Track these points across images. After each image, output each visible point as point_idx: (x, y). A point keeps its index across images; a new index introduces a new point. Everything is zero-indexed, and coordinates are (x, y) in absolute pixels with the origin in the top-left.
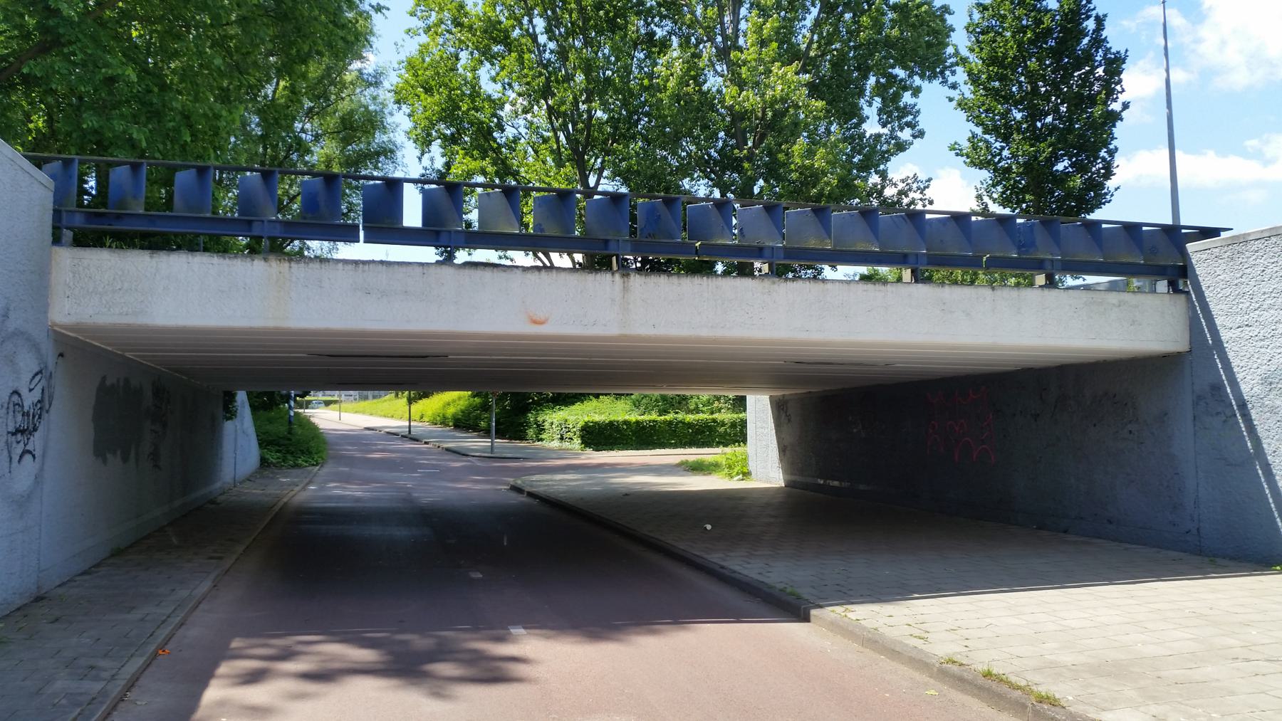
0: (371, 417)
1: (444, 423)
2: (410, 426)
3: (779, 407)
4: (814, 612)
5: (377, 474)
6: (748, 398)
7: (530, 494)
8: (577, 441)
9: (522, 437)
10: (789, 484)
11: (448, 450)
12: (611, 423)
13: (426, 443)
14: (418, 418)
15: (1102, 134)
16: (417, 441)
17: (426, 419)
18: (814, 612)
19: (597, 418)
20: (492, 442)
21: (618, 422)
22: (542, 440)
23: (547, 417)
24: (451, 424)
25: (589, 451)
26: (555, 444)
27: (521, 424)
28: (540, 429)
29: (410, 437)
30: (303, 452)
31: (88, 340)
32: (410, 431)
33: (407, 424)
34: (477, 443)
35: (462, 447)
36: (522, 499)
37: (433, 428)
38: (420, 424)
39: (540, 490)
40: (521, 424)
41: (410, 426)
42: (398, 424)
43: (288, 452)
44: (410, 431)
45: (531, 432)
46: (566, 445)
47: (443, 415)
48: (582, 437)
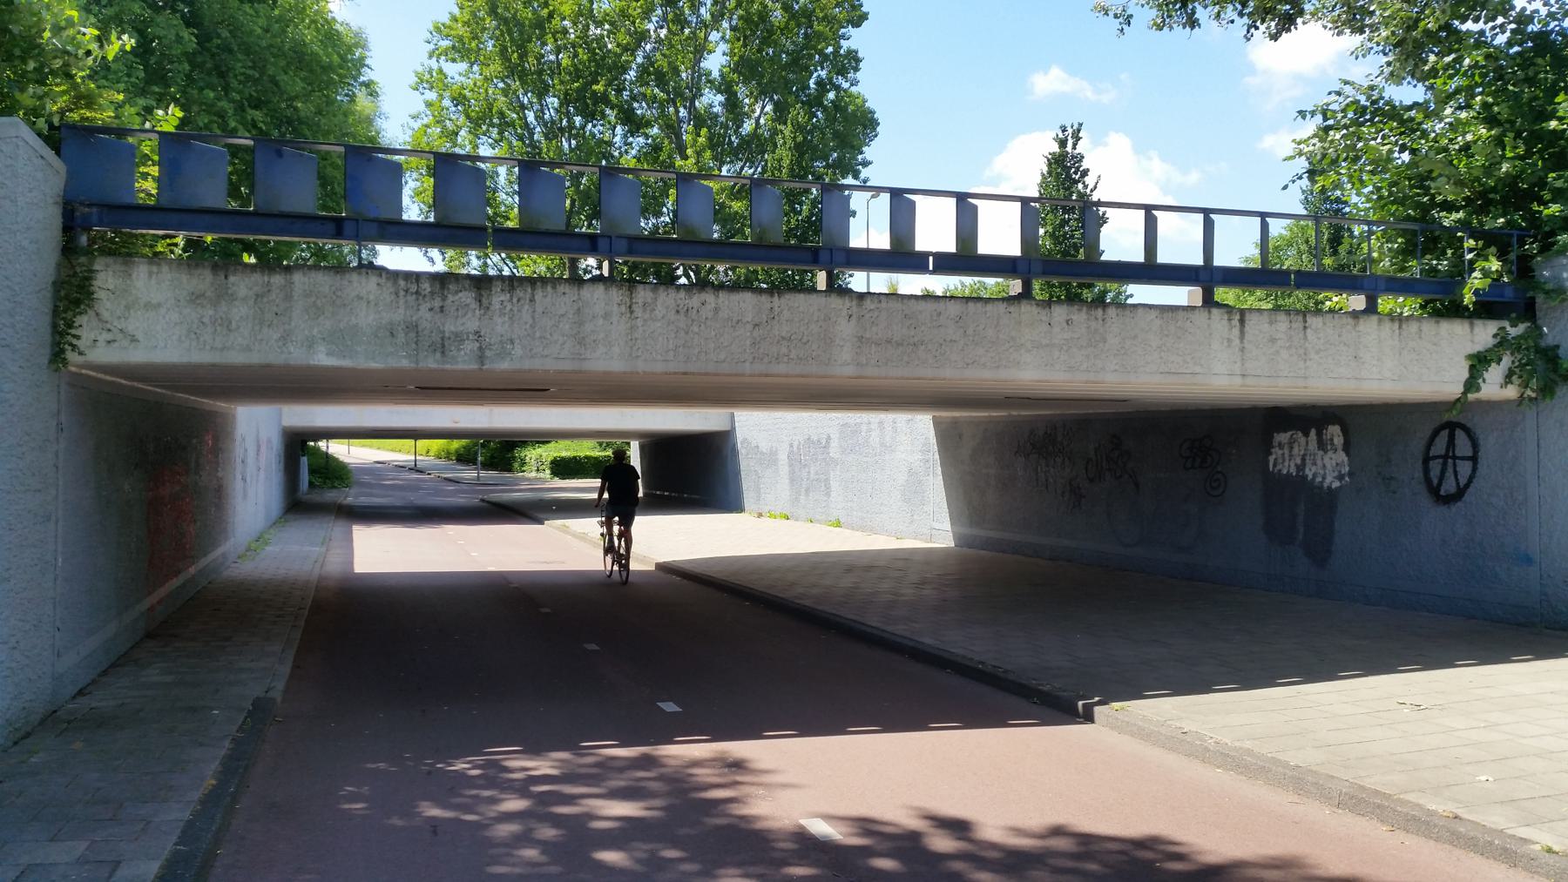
0: (378, 451)
1: (448, 458)
2: (416, 460)
3: (642, 448)
4: (546, 522)
5: (390, 493)
6: (632, 443)
7: (488, 502)
8: (548, 472)
9: (510, 470)
10: (961, 541)
11: (446, 479)
12: (575, 458)
13: (429, 474)
14: (424, 453)
15: (1422, 54)
16: (422, 472)
17: (431, 453)
18: (546, 522)
19: (564, 454)
20: (478, 473)
21: (580, 457)
22: (524, 471)
23: (528, 453)
24: (454, 458)
25: (556, 479)
26: (534, 474)
27: (509, 459)
28: (523, 463)
29: (415, 469)
30: (337, 478)
31: (84, 371)
32: (416, 465)
33: (413, 458)
34: (469, 474)
35: (457, 477)
36: (484, 504)
37: (438, 462)
38: (427, 458)
39: (494, 500)
40: (509, 459)
41: (416, 460)
42: (440, 267)
43: (327, 478)
44: (416, 465)
45: (516, 465)
46: (541, 475)
47: (447, 450)
48: (552, 469)
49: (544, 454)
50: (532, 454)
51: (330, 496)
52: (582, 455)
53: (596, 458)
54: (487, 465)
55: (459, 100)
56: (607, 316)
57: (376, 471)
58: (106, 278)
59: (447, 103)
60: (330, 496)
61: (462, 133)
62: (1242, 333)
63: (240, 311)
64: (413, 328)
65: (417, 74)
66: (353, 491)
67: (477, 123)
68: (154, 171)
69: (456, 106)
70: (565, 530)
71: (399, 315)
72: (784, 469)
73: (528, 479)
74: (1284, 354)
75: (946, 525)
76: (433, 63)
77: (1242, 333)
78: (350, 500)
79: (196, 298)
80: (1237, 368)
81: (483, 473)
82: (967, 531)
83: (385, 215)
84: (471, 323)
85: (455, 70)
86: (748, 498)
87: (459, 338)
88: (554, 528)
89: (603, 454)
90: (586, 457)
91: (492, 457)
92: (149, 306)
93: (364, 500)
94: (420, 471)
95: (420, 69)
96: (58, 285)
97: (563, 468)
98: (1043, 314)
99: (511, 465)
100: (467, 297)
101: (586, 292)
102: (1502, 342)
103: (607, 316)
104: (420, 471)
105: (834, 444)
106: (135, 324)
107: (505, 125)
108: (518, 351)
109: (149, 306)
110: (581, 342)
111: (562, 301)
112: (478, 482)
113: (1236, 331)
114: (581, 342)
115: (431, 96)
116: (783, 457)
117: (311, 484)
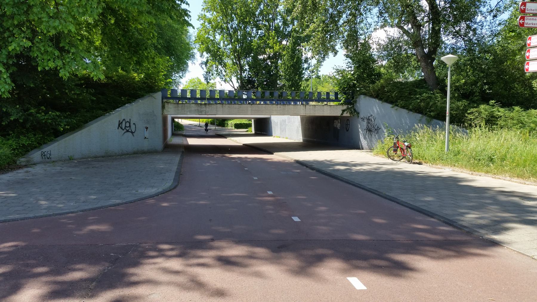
8: (234, 127)
10: (303, 140)
19: (238, 122)
26: (230, 128)
45: (226, 125)
48: (234, 126)
49: (233, 122)
50: (230, 122)
51: (179, 132)
52: (242, 123)
53: (246, 124)
54: (218, 125)
55: (210, 22)
56: (220, 108)
57: (190, 126)
58: (166, 105)
59: (206, 24)
60: (179, 132)
61: (211, 32)
62: (305, 108)
63: (180, 108)
64: (198, 110)
65: (198, 16)
66: (185, 131)
67: (215, 29)
68: (168, 93)
69: (209, 24)
70: (230, 139)
71: (196, 108)
72: (279, 126)
73: (229, 129)
74: (312, 111)
75: (301, 138)
76: (203, 13)
77: (305, 108)
78: (184, 133)
79: (175, 107)
80: (305, 113)
81: (217, 127)
82: (304, 138)
83: (195, 97)
84: (204, 109)
85: (208, 15)
86: (273, 134)
87: (203, 111)
88: (232, 140)
89: (248, 122)
90: (244, 123)
91: (220, 123)
92: (170, 108)
93: (188, 134)
94: (201, 127)
95: (199, 14)
96: (162, 106)
97: (238, 126)
98: (277, 106)
99: (224, 125)
100: (204, 106)
101: (217, 105)
102: (348, 108)
103: (220, 108)
104: (201, 127)
105: (287, 120)
106: (169, 110)
107: (222, 29)
108: (209, 112)
109: (170, 108)
110: (217, 111)
111: (215, 106)
112: (215, 130)
113: (304, 108)
114: (217, 111)
115: (202, 22)
116: (279, 123)
117: (174, 129)
